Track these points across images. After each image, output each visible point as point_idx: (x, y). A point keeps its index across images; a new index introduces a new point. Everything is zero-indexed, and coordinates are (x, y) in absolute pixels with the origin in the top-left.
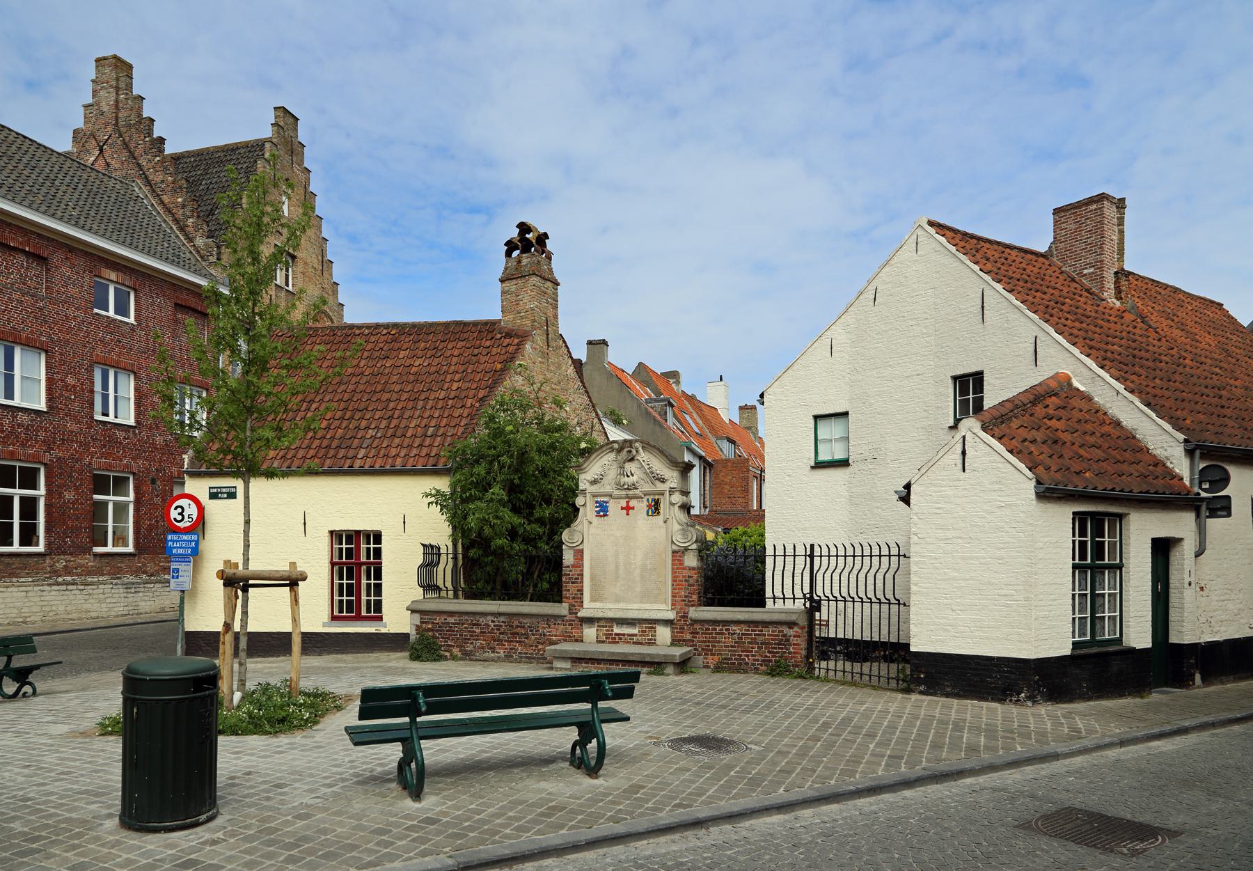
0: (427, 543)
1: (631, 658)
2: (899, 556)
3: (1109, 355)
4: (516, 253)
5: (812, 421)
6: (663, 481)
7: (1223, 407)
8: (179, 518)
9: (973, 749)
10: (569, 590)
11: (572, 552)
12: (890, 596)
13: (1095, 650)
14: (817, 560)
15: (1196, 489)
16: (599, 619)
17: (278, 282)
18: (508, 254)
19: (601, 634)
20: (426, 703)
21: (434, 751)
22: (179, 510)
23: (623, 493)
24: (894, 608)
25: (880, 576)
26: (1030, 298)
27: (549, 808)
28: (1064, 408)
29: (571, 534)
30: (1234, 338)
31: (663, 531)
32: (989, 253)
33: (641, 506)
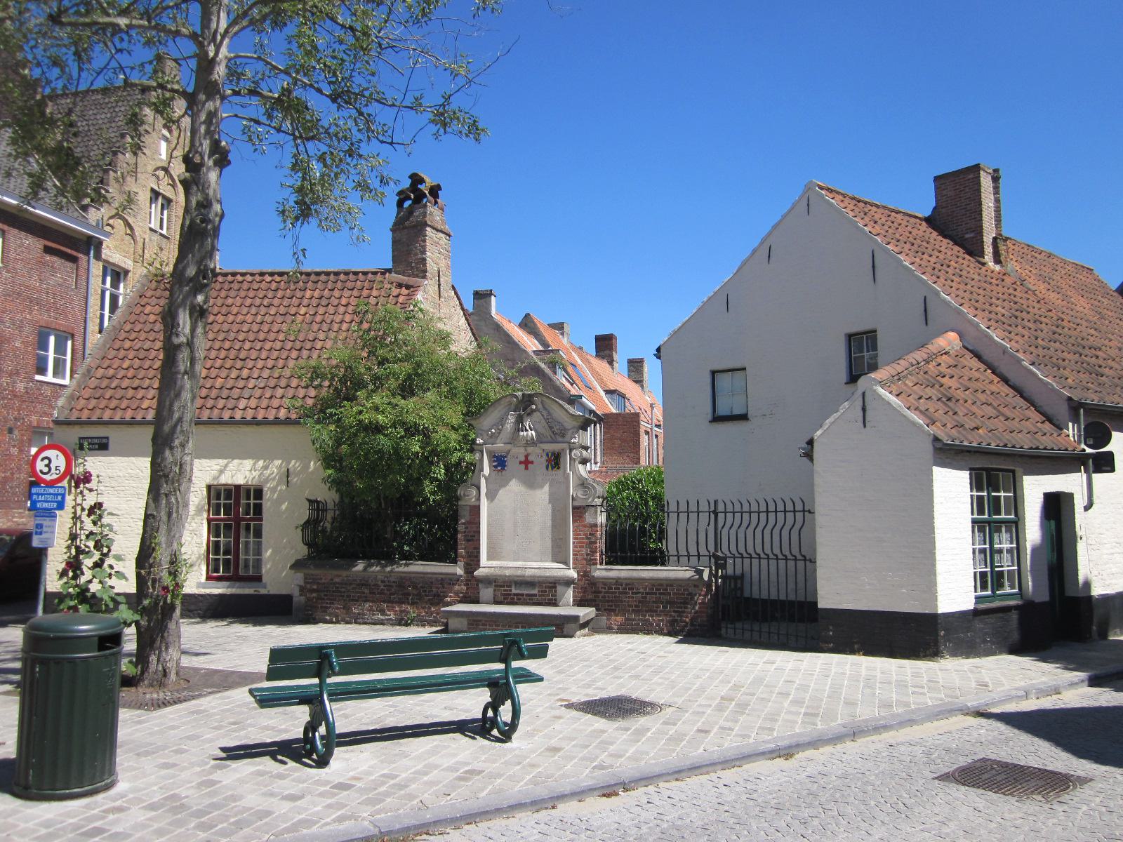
0: (313, 498)
2: (804, 511)
3: (993, 316)
4: (407, 204)
7: (1100, 366)
8: (46, 470)
9: (886, 705)
12: (795, 551)
13: (997, 604)
14: (721, 516)
15: (1083, 446)
17: (152, 226)
18: (400, 204)
20: (339, 664)
21: (348, 715)
22: (46, 462)
24: (801, 564)
25: (785, 533)
26: (917, 260)
27: (466, 772)
28: (956, 366)
30: (1106, 301)
32: (877, 217)
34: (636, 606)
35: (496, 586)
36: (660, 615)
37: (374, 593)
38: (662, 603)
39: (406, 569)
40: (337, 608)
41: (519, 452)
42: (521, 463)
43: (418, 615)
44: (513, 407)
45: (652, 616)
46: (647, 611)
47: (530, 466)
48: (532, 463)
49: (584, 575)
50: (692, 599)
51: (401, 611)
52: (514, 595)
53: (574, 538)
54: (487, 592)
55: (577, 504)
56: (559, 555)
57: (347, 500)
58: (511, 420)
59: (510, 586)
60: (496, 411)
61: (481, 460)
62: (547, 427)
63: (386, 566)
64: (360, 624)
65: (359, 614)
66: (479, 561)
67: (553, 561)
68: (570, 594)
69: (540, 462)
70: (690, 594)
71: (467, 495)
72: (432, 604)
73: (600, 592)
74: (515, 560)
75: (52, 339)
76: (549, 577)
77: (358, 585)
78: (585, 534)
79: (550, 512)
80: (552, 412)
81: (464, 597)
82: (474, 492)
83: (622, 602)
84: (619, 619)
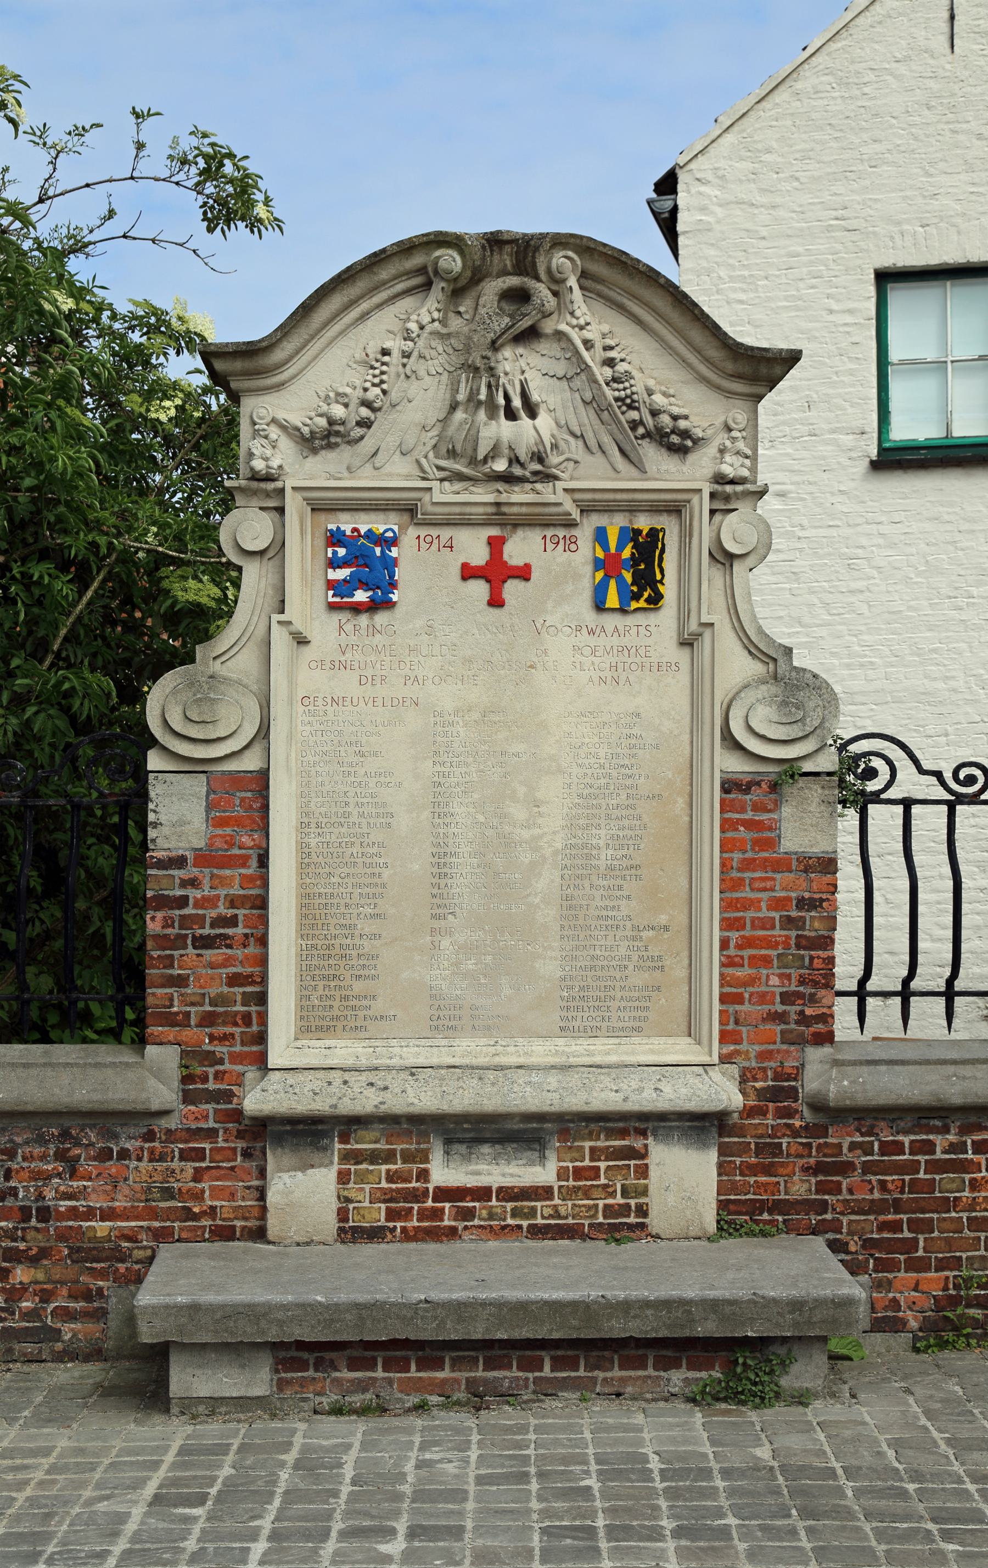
1: (616, 1328)
5: (872, 290)
6: (679, 443)
10: (189, 980)
11: (198, 785)
16: (351, 1124)
19: (361, 1194)
23: (483, 495)
29: (206, 694)
31: (677, 687)
33: (562, 568)
42: (468, 573)
47: (480, 589)
48: (524, 573)
52: (444, 1194)
73: (845, 1168)
75: (860, 771)
78: (777, 904)
83: (946, 1205)
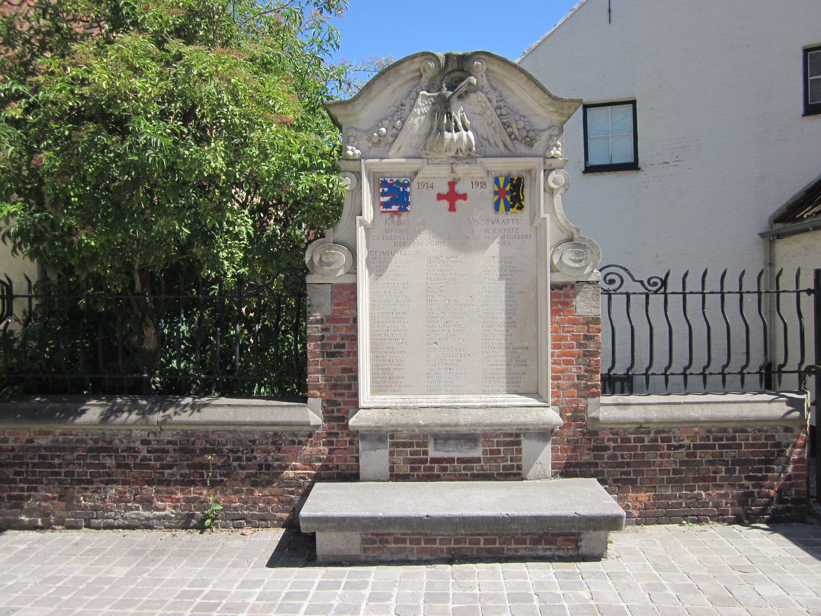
34: (675, 472)
35: (393, 445)
36: (720, 487)
37: (127, 466)
38: (725, 463)
39: (196, 417)
40: (46, 499)
41: (437, 175)
42: (440, 197)
43: (225, 508)
44: (424, 81)
45: (706, 489)
46: (695, 480)
47: (459, 203)
48: (464, 197)
49: (575, 416)
50: (781, 453)
51: (189, 501)
52: (434, 460)
53: (555, 347)
54: (374, 458)
55: (559, 279)
56: (521, 381)
57: (53, 277)
58: (423, 107)
59: (425, 444)
60: (389, 90)
61: (357, 190)
62: (497, 122)
63: (151, 412)
64: (98, 528)
65: (95, 509)
66: (356, 395)
67: (509, 392)
68: (543, 457)
69: (481, 198)
70: (778, 445)
71: (326, 266)
72: (255, 484)
73: (606, 448)
74: (430, 392)
76: (509, 425)
77: (90, 450)
78: (576, 338)
79: (502, 296)
80: (506, 93)
81: (326, 467)
82: (342, 256)
84: (643, 496)
